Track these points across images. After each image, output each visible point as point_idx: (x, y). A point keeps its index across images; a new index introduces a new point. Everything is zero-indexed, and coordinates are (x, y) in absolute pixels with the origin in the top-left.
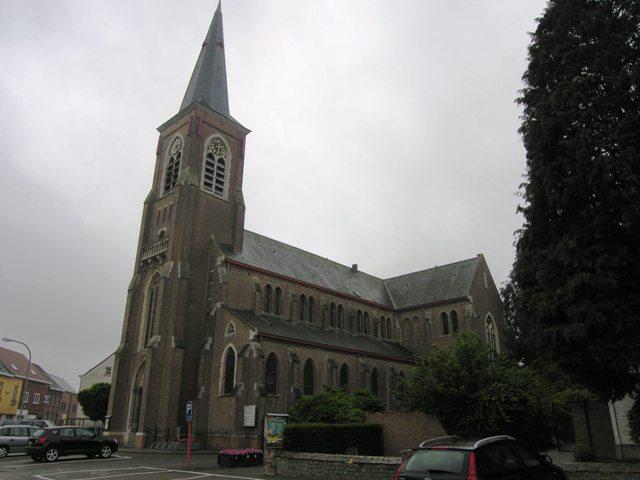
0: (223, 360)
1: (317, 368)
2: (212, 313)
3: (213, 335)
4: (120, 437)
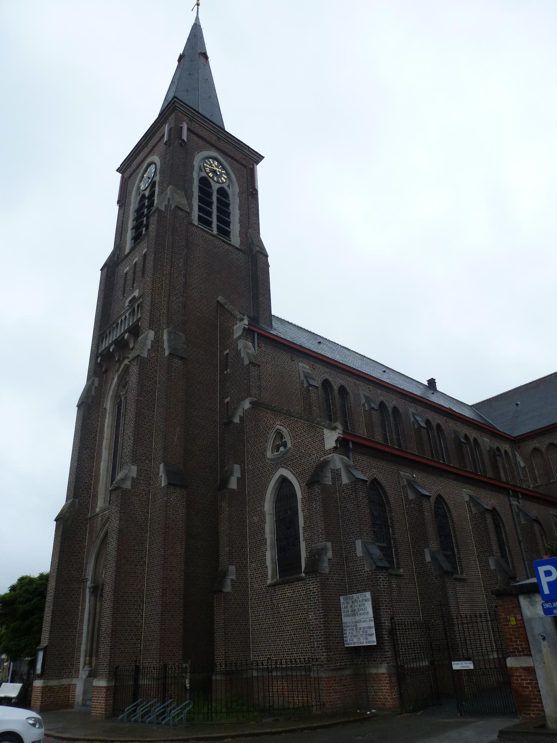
0: (268, 506)
1: (455, 514)
2: (237, 420)
3: (242, 462)
4: (69, 689)
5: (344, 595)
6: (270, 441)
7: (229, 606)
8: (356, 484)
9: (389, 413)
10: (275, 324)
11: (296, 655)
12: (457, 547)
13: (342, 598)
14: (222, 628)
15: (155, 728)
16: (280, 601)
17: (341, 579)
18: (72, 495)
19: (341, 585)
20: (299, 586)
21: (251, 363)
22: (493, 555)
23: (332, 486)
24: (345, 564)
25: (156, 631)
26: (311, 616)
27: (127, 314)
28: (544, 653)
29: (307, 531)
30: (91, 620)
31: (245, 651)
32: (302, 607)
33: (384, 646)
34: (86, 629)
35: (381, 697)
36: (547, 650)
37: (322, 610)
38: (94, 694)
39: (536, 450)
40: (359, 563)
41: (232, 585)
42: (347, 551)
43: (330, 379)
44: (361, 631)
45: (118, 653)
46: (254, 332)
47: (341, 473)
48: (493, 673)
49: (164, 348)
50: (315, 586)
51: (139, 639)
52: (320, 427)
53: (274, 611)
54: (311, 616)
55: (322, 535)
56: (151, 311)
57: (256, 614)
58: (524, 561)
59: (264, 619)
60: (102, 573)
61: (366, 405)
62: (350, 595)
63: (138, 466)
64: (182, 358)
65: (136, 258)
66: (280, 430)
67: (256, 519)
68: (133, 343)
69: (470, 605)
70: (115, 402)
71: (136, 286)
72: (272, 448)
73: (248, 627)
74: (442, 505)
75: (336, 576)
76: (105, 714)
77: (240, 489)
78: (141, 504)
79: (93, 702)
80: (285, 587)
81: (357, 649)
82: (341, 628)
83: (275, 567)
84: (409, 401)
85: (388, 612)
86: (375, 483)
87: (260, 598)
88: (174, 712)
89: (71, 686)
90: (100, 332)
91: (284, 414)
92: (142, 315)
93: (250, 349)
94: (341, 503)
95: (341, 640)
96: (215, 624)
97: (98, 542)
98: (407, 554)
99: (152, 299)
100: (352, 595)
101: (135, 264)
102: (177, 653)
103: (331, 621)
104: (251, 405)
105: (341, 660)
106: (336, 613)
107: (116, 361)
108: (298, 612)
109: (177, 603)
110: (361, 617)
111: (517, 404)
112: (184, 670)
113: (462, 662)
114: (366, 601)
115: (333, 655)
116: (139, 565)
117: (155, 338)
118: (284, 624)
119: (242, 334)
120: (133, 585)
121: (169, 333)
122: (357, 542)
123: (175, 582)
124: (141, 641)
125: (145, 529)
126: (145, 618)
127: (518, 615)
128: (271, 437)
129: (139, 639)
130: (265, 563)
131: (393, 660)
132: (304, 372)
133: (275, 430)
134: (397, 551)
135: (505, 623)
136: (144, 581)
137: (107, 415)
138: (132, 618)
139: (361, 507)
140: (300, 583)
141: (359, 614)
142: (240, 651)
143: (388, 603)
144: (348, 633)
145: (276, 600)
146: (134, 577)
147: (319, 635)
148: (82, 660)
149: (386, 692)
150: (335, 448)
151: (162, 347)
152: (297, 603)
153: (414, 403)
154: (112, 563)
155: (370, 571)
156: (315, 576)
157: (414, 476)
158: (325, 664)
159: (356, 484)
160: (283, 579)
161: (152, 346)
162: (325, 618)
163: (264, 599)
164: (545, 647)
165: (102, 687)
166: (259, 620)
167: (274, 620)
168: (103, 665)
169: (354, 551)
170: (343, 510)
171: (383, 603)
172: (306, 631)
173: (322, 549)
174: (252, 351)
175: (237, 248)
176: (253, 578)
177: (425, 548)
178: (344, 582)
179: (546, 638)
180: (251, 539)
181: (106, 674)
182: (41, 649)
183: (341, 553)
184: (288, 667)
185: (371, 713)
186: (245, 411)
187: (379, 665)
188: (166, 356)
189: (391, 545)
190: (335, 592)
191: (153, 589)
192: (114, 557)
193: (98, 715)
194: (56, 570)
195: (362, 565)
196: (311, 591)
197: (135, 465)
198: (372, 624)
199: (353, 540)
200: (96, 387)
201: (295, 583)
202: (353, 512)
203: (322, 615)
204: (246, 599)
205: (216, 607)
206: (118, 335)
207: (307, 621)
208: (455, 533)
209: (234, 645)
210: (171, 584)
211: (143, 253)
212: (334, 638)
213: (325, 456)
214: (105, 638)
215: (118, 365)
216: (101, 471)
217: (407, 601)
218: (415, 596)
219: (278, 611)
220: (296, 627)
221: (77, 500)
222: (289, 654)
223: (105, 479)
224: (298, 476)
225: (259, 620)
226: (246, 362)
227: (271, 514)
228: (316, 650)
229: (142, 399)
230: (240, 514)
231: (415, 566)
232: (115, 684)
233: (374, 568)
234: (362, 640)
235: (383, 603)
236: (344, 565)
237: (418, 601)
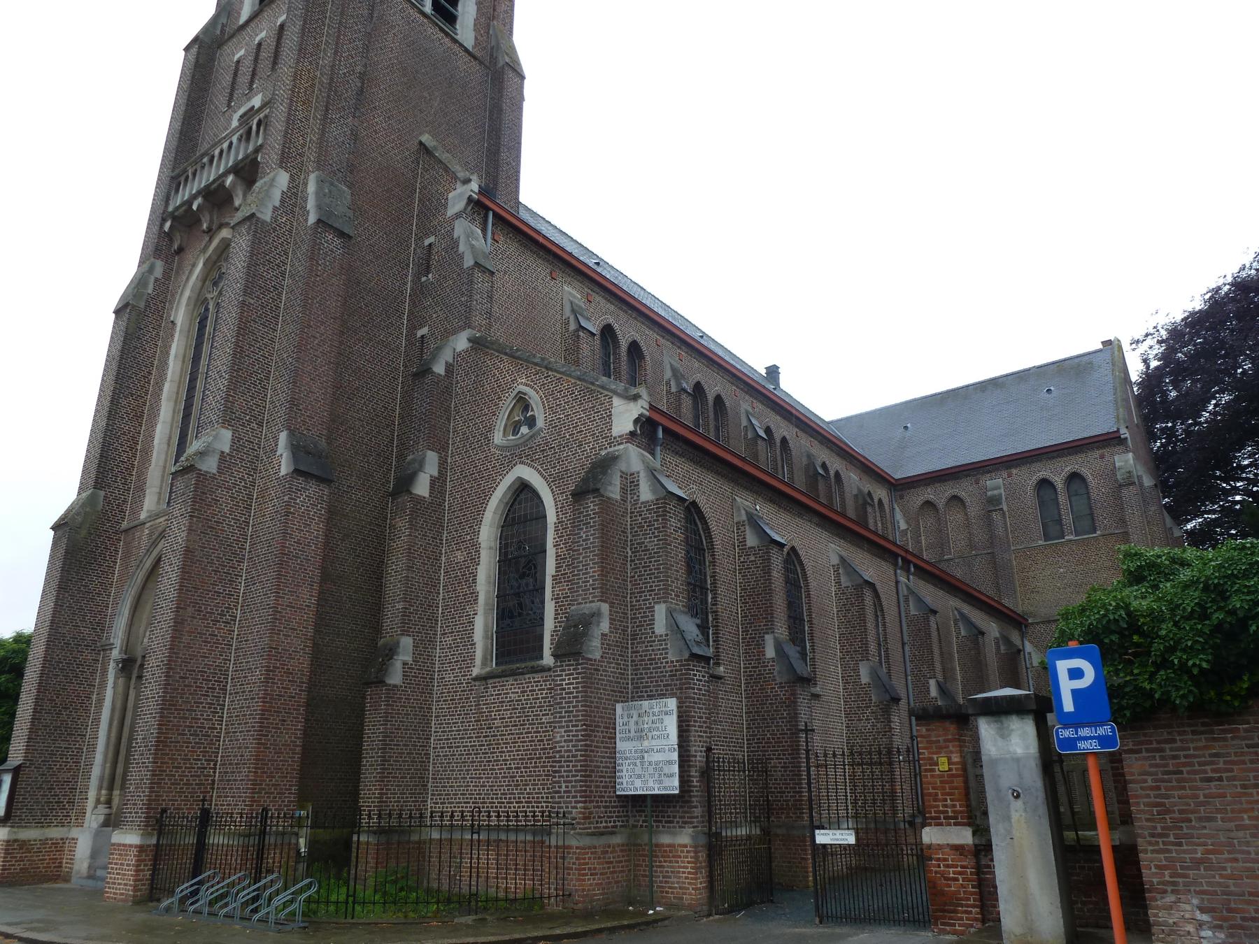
0: (488, 533)
1: (813, 584)
2: (439, 369)
3: (442, 449)
4: (59, 846)
5: (622, 702)
6: (502, 413)
7: (394, 710)
8: (666, 503)
9: (707, 405)
10: (521, 210)
11: (517, 805)
12: (812, 639)
13: (619, 707)
14: (379, 749)
15: (237, 927)
16: (494, 707)
17: (620, 673)
18: (91, 482)
19: (619, 683)
20: (535, 682)
21: (477, 264)
22: (868, 660)
23: (620, 503)
24: (630, 646)
25: (248, 748)
26: (560, 735)
27: (235, 139)
28: (1013, 820)
29: (561, 582)
30: (115, 723)
31: (418, 794)
32: (537, 719)
33: (690, 796)
34: (105, 738)
36: (1021, 816)
37: (582, 726)
38: (113, 859)
39: (929, 504)
40: (657, 645)
41: (404, 672)
42: (635, 622)
43: (616, 327)
44: (651, 768)
45: (167, 784)
46: (487, 209)
47: (638, 481)
48: (843, 852)
49: (308, 208)
50: (572, 681)
51: (213, 761)
52: (606, 393)
53: (481, 725)
54: (560, 735)
55: (593, 589)
56: (286, 132)
57: (444, 728)
58: (906, 676)
59: (461, 738)
60: (144, 637)
61: (673, 383)
62: (637, 703)
63: (234, 431)
64: (342, 234)
65: (261, 32)
66: (525, 394)
67: (460, 557)
68: (241, 196)
69: (821, 740)
70: (195, 314)
71: (257, 87)
72: (506, 425)
73: (427, 750)
74: (795, 566)
75: (612, 665)
76: (134, 896)
77: (435, 497)
78: (235, 505)
79: (110, 873)
80: (507, 681)
81: (638, 801)
82: (612, 760)
83: (490, 646)
84: (742, 389)
85: (702, 736)
86: (692, 510)
87: (454, 700)
88: (278, 901)
89: (67, 842)
90: (173, 172)
91: (536, 364)
92: (265, 139)
93: (477, 239)
94: (633, 536)
95: (610, 782)
96: (365, 742)
97: (140, 576)
98: (733, 641)
99: (290, 109)
101: (260, 44)
102: (286, 789)
103: (596, 747)
104: (471, 344)
105: (608, 817)
106: (607, 732)
107: (204, 232)
108: (528, 728)
109: (294, 697)
110: (654, 743)
111: (906, 428)
112: (299, 822)
113: (834, 831)
114: (666, 714)
115: (595, 807)
116: (223, 622)
117: (289, 188)
118: (498, 748)
119: (465, 209)
120: (207, 657)
121: (320, 181)
122: (657, 607)
123: (294, 659)
124: (215, 765)
125: (239, 555)
126: (226, 721)
128: (505, 406)
129: (213, 761)
130: (471, 637)
131: (703, 822)
132: (571, 303)
133: (515, 393)
134: (717, 633)
135: (928, 767)
136: (231, 653)
137: (177, 335)
138: (200, 719)
139: (671, 545)
140: (538, 677)
141: (650, 738)
142: (409, 794)
143: (705, 722)
144: (625, 771)
145: (488, 704)
146: (210, 642)
147: (571, 771)
148: (92, 795)
149: (686, 878)
150: (632, 434)
151: (304, 208)
152: (528, 712)
153: (751, 396)
154: (167, 613)
155: (677, 661)
156: (575, 663)
157: (758, 507)
158: (578, 823)
159: (666, 503)
160: (503, 667)
161: (282, 201)
162: (586, 740)
163: (463, 703)
164: (1016, 811)
165: (131, 846)
166: (449, 739)
167: (478, 741)
168: (134, 804)
169: (651, 624)
170: (636, 548)
171: (695, 721)
172: (540, 763)
173: (593, 615)
174: (480, 243)
175: (466, 50)
176: (444, 664)
177: (768, 633)
178: (625, 679)
179: (1022, 795)
180: (447, 592)
181: (141, 822)
182: (7, 771)
183: (624, 626)
184: (483, 825)
185: (656, 913)
186: (457, 355)
187: (678, 829)
188: (309, 224)
189: (708, 623)
190: (608, 695)
191: (248, 669)
192: (172, 601)
193: (118, 896)
194: (48, 623)
195: (663, 649)
196: (564, 689)
197: (227, 428)
198: (675, 756)
199: (650, 603)
200: (156, 280)
201: (527, 676)
202: (654, 553)
203: (582, 735)
204: (428, 701)
205: (370, 710)
206: (211, 179)
207: (544, 745)
208: (810, 615)
209: (399, 782)
210: (285, 661)
211: (278, 24)
213: (610, 447)
214: (142, 755)
215: (207, 239)
216: (156, 442)
217: (725, 722)
218: (740, 716)
219: (490, 724)
220: (522, 755)
221: (102, 493)
222: (504, 803)
223: (163, 457)
224: (552, 481)
225: (449, 739)
226: (468, 262)
227: (490, 548)
228: (563, 797)
229: (252, 301)
230: (431, 544)
231: (745, 664)
232: (158, 840)
233: (686, 655)
234: (651, 784)
235: (695, 721)
236: (628, 648)
237: (743, 724)
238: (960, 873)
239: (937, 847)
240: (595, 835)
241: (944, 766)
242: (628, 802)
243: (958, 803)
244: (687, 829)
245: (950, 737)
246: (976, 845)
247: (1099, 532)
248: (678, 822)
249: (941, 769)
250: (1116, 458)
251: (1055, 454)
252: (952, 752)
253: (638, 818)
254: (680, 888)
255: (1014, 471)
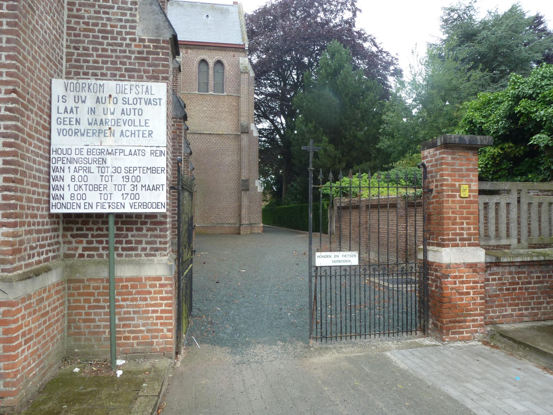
35: (141, 328)
44: (118, 179)
100: (101, 82)
110: (124, 141)
114: (148, 102)
127: (473, 183)
135: (450, 193)
149: (158, 318)
155: (150, 41)
187: (143, 258)
212: (32, 186)
234: (117, 197)
238: (472, 288)
239: (455, 266)
240: (29, 278)
241: (465, 193)
242: (58, 223)
243: (472, 227)
244: (159, 258)
245: (471, 167)
246: (486, 263)
247: (225, 94)
248: (144, 249)
249: (462, 196)
250: (240, 58)
251: (212, 48)
252: (472, 181)
253: (74, 245)
254: (148, 331)
255: (189, 51)
